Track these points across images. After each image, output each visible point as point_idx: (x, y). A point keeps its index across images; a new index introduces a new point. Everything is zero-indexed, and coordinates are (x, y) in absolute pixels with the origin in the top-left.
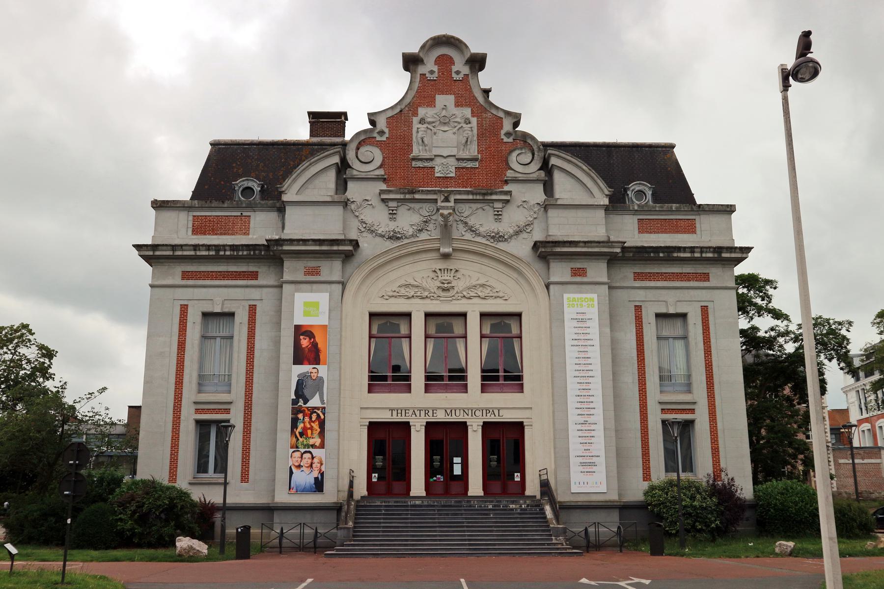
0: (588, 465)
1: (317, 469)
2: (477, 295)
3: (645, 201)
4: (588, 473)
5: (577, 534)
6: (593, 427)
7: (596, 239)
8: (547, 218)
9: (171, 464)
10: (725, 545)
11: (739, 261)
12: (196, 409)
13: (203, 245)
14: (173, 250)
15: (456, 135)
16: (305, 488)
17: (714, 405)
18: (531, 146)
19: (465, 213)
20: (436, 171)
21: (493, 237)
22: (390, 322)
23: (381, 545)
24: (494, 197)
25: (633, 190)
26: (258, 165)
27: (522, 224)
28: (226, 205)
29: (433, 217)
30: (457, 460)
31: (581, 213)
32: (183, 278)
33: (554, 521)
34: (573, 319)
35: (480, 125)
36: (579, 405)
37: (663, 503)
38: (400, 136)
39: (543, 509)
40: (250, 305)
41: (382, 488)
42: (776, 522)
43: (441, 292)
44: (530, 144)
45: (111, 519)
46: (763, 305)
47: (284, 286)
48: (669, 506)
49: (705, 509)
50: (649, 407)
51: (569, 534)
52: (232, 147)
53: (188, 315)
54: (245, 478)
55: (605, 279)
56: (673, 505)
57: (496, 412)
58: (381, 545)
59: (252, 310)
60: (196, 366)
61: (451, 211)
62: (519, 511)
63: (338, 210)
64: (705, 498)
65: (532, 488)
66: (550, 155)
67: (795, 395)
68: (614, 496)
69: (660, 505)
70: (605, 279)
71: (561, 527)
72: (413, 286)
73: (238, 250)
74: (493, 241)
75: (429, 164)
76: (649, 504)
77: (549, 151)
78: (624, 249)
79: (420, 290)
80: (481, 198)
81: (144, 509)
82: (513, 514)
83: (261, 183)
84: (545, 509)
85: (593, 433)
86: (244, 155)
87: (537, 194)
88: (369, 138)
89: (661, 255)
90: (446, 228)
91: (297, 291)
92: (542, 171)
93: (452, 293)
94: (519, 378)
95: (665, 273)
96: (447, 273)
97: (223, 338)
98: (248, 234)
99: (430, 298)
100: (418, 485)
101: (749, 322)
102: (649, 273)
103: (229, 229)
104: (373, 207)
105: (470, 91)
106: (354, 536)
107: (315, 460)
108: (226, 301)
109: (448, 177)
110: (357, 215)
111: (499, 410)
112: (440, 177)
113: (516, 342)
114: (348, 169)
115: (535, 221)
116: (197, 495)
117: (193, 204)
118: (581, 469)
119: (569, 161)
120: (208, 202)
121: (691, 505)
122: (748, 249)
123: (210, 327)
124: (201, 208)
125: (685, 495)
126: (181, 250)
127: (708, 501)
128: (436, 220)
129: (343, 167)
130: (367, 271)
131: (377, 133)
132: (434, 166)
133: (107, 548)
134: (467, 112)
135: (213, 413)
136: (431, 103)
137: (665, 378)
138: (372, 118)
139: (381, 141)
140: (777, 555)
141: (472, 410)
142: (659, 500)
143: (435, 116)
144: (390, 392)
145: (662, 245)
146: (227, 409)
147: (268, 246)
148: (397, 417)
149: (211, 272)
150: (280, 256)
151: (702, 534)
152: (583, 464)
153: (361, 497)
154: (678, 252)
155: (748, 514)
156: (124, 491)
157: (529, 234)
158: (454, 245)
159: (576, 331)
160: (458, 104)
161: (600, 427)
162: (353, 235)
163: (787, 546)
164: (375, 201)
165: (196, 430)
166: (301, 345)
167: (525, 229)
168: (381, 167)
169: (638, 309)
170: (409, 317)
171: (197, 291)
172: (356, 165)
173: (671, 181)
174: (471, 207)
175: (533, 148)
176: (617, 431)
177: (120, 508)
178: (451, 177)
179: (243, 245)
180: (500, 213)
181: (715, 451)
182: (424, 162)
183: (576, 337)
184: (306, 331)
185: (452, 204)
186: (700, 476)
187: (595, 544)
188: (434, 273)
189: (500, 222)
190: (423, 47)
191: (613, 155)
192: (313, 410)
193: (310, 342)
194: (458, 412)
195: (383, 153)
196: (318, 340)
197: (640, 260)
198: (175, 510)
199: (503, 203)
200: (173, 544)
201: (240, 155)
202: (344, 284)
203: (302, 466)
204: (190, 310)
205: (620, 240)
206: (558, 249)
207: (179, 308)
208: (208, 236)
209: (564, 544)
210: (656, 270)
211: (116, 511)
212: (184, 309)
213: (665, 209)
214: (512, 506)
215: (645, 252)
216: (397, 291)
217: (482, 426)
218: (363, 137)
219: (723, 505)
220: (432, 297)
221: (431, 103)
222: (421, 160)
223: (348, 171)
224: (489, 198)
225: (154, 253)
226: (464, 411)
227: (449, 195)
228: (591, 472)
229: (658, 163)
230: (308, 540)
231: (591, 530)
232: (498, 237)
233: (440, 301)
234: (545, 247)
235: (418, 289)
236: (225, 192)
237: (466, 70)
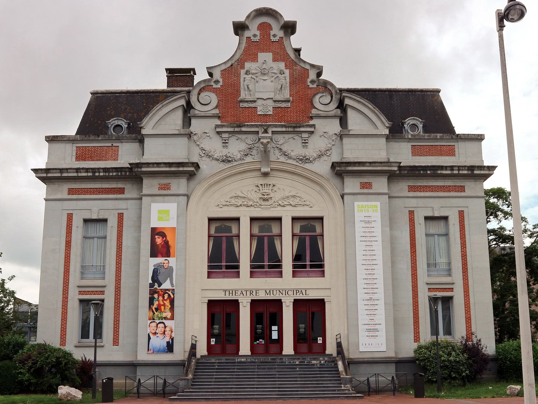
0: (372, 331)
1: (168, 335)
2: (289, 204)
3: (417, 132)
4: (373, 337)
5: (362, 383)
6: (376, 302)
7: (379, 161)
8: (342, 144)
10: (472, 388)
11: (486, 176)
12: (79, 292)
13: (83, 169)
14: (61, 173)
15: (273, 83)
16: (159, 350)
17: (468, 285)
18: (331, 91)
20: (258, 110)
21: (301, 160)
22: (224, 224)
23: (212, 392)
24: (302, 129)
25: (408, 124)
26: (126, 109)
27: (323, 149)
28: (100, 138)
30: (275, 328)
31: (368, 141)
32: (69, 194)
33: (344, 373)
34: (362, 221)
35: (291, 75)
36: (366, 286)
37: (427, 359)
38: (231, 84)
39: (336, 364)
40: (118, 213)
41: (218, 349)
42: (511, 371)
43: (262, 202)
44: (329, 89)
45: (14, 372)
46: (508, 211)
47: (144, 198)
48: (431, 361)
49: (458, 362)
50: (419, 287)
51: (355, 382)
52: (106, 95)
54: (116, 342)
55: (386, 191)
56: (434, 360)
57: (304, 292)
58: (212, 392)
59: (121, 217)
60: (79, 259)
61: (269, 140)
62: (318, 366)
63: (184, 140)
64: (458, 355)
65: (331, 349)
66: (344, 97)
67: (531, 278)
68: (391, 354)
69: (425, 360)
70: (386, 191)
71: (348, 377)
72: (241, 197)
73: (109, 172)
74: (301, 163)
75: (253, 105)
76: (418, 360)
77: (344, 94)
78: (400, 168)
80: (292, 130)
81: (38, 365)
82: (314, 368)
84: (338, 364)
85: (376, 307)
86: (116, 101)
87: (334, 126)
88: (207, 86)
89: (429, 172)
90: (266, 153)
91: (153, 202)
92: (338, 109)
94: (322, 266)
96: (267, 187)
97: (99, 238)
98: (117, 160)
99: (253, 206)
100: (245, 348)
101: (498, 224)
102: (420, 186)
103: (103, 156)
104: (211, 138)
105: (284, 49)
106: (192, 385)
107: (167, 329)
109: (267, 115)
111: (306, 290)
112: (261, 115)
113: (319, 238)
114: (192, 110)
115: (333, 147)
116: (78, 355)
117: (76, 138)
118: (367, 334)
119: (359, 102)
120: (87, 136)
121: (448, 359)
122: (493, 168)
123: (89, 229)
124: (82, 141)
125: (443, 352)
126: (67, 173)
127: (460, 357)
128: (258, 147)
129: (188, 108)
131: (214, 82)
132: (256, 106)
133: (10, 394)
134: (282, 65)
135: (92, 294)
136: (255, 59)
137: (431, 265)
138: (210, 71)
140: (508, 396)
141: (285, 291)
142: (425, 356)
144: (224, 277)
145: (429, 165)
146: (102, 291)
147: (131, 168)
148: (229, 296)
149: (90, 189)
150: (141, 176)
151: (456, 380)
152: (369, 330)
153: (201, 356)
154: (441, 170)
155: (491, 365)
156: (24, 352)
157: (329, 157)
158: (272, 166)
159: (364, 230)
160: (275, 60)
161: (382, 302)
162: (195, 159)
163: (515, 388)
164: (212, 134)
165: (80, 309)
166: (156, 243)
167: (326, 154)
168: (216, 107)
169: (411, 213)
170: (238, 221)
172: (197, 106)
173: (437, 117)
174: (284, 137)
175: (332, 92)
176: (394, 305)
177: (20, 365)
178: (270, 115)
179: (112, 168)
181: (468, 320)
182: (249, 103)
183: (364, 234)
184: (160, 232)
185: (270, 135)
186: (457, 338)
187: (375, 389)
188: (257, 187)
190: (248, 17)
191: (394, 98)
192: (165, 291)
193: (163, 240)
194: (275, 292)
195: (218, 97)
196: (168, 239)
197: (413, 176)
198: (61, 366)
199: (309, 134)
200: (55, 392)
201: (113, 101)
202: (188, 196)
203: (157, 333)
204: (74, 217)
205: (398, 161)
206: (350, 168)
207: (66, 215)
208: (87, 162)
209: (351, 390)
210: (425, 184)
211: (17, 367)
212: (70, 217)
213: (432, 137)
214: (314, 362)
215: (416, 170)
216: (229, 201)
217: (293, 303)
218: (202, 86)
219: (471, 359)
220: (255, 206)
221: (255, 59)
222: (247, 102)
223: (192, 111)
224: (298, 130)
225: (47, 175)
226: (279, 291)
227: (267, 128)
228: (375, 336)
229: (427, 103)
230: (160, 388)
231: (372, 379)
232: (305, 160)
234: (340, 166)
235: (245, 199)
236: (101, 128)
237: (281, 34)
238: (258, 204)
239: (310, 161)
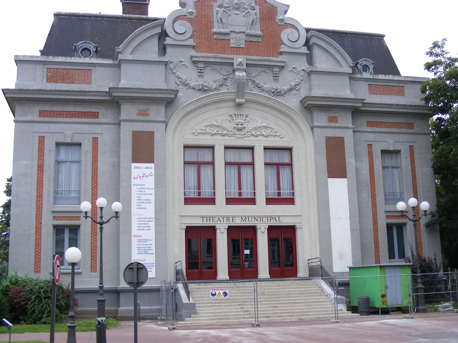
9: (36, 258)
19: (253, 74)
20: (231, 42)
27: (293, 84)
29: (230, 76)
38: (205, 16)
40: (93, 138)
47: (122, 123)
53: (45, 144)
55: (351, 125)
57: (277, 219)
59: (95, 141)
70: (351, 125)
72: (216, 126)
74: (273, 95)
75: (226, 37)
79: (221, 129)
83: (96, 45)
93: (244, 132)
95: (386, 122)
96: (240, 118)
98: (91, 84)
99: (228, 135)
104: (186, 67)
108: (74, 134)
109: (240, 48)
110: (175, 72)
115: (302, 82)
128: (232, 78)
130: (182, 114)
132: (230, 39)
139: (191, 18)
141: (260, 217)
143: (230, 3)
146: (78, 217)
148: (207, 223)
149: (62, 111)
164: (187, 62)
169: (370, 146)
171: (51, 126)
174: (257, 70)
178: (242, 48)
180: (277, 75)
189: (277, 81)
194: (250, 219)
204: (46, 140)
212: (42, 140)
216: (204, 129)
217: (185, 229)
220: (229, 135)
226: (255, 218)
232: (277, 93)
233: (236, 137)
238: (232, 134)
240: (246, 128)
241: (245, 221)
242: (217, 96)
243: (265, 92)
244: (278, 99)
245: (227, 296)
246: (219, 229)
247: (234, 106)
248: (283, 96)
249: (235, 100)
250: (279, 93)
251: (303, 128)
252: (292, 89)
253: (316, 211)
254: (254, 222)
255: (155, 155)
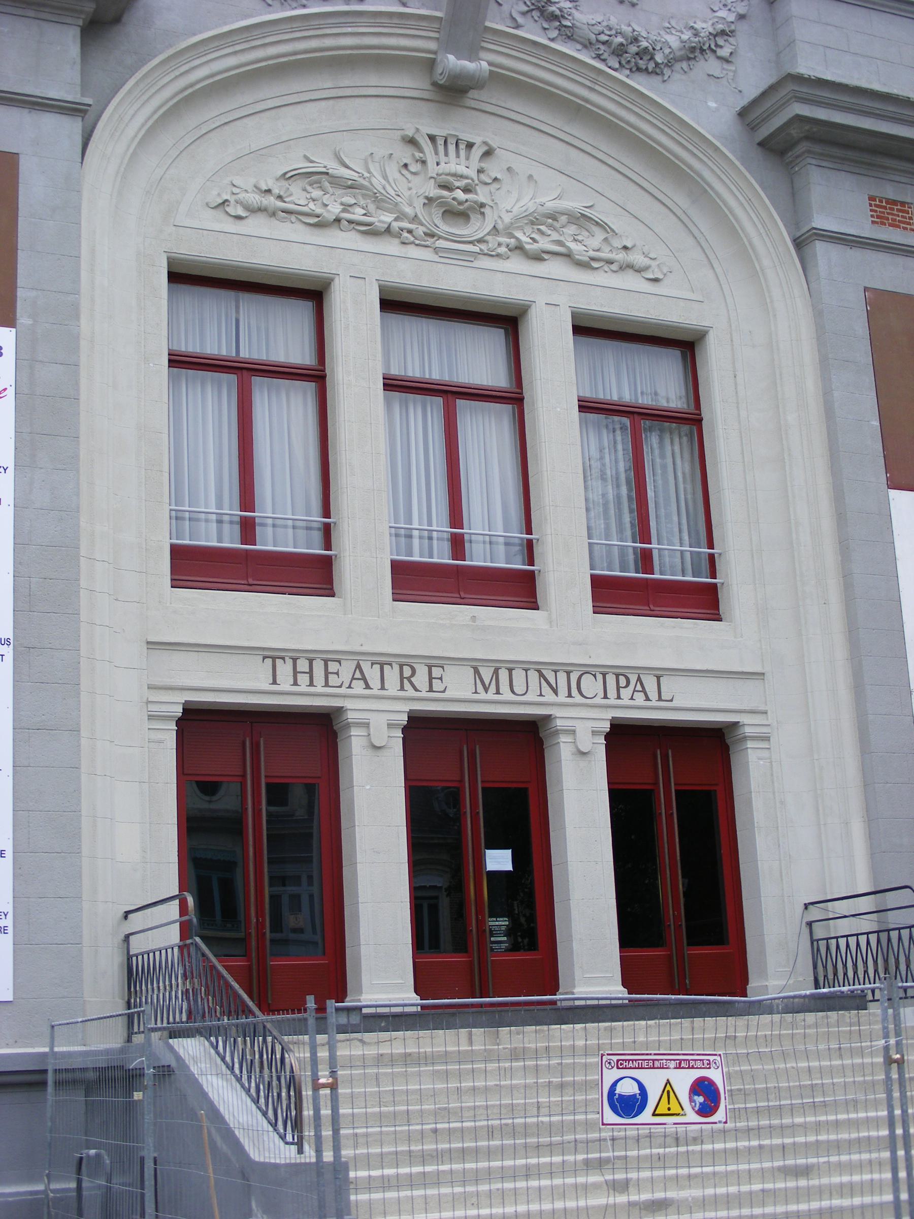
27: (705, 27)
57: (650, 684)
72: (337, 182)
74: (617, 66)
93: (476, 228)
96: (458, 156)
99: (399, 236)
115: (742, 28)
141: (568, 673)
157: (725, 66)
167: (713, 47)
194: (519, 675)
216: (276, 191)
220: (405, 234)
226: (541, 675)
238: (420, 230)
239: (657, 64)
240: (487, 210)
241: (493, 688)
242: (350, 30)
243: (579, 47)
244: (639, 83)
245: (720, 1115)
246: (359, 725)
247: (426, 95)
248: (659, 78)
249: (431, 64)
250: (646, 57)
251: (756, 241)
252: (702, 51)
253: (841, 653)
254: (541, 699)
255: (21, 281)
